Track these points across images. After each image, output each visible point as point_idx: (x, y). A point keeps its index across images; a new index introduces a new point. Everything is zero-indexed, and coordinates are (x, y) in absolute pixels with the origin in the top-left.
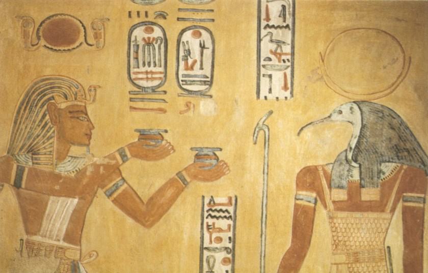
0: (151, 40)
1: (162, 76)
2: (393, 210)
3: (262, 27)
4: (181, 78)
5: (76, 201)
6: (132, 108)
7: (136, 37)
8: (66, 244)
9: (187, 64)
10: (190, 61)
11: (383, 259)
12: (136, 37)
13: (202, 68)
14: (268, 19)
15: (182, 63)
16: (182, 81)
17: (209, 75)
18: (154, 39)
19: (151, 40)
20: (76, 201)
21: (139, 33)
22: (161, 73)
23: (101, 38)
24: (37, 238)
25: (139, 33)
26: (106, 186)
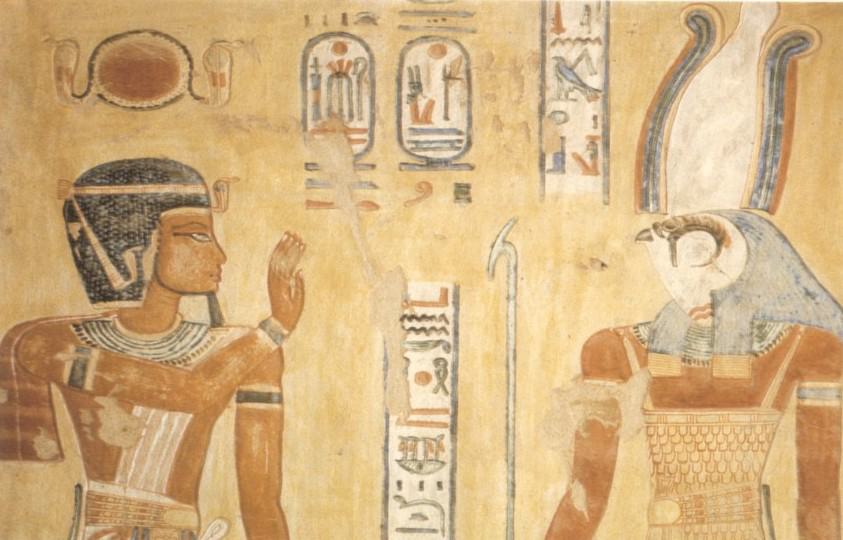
0: (345, 64)
1: (365, 136)
2: (779, 404)
3: (548, 43)
4: (406, 137)
5: (191, 416)
6: (309, 204)
7: (316, 60)
8: (167, 501)
9: (415, 109)
10: (422, 103)
11: (751, 519)
12: (316, 60)
13: (446, 118)
14: (559, 28)
15: (406, 109)
16: (409, 142)
17: (463, 127)
18: (349, 64)
19: (345, 64)
20: (191, 416)
21: (324, 52)
22: (363, 131)
23: (223, 85)
24: (112, 489)
25: (324, 52)
26: (153, 480)
